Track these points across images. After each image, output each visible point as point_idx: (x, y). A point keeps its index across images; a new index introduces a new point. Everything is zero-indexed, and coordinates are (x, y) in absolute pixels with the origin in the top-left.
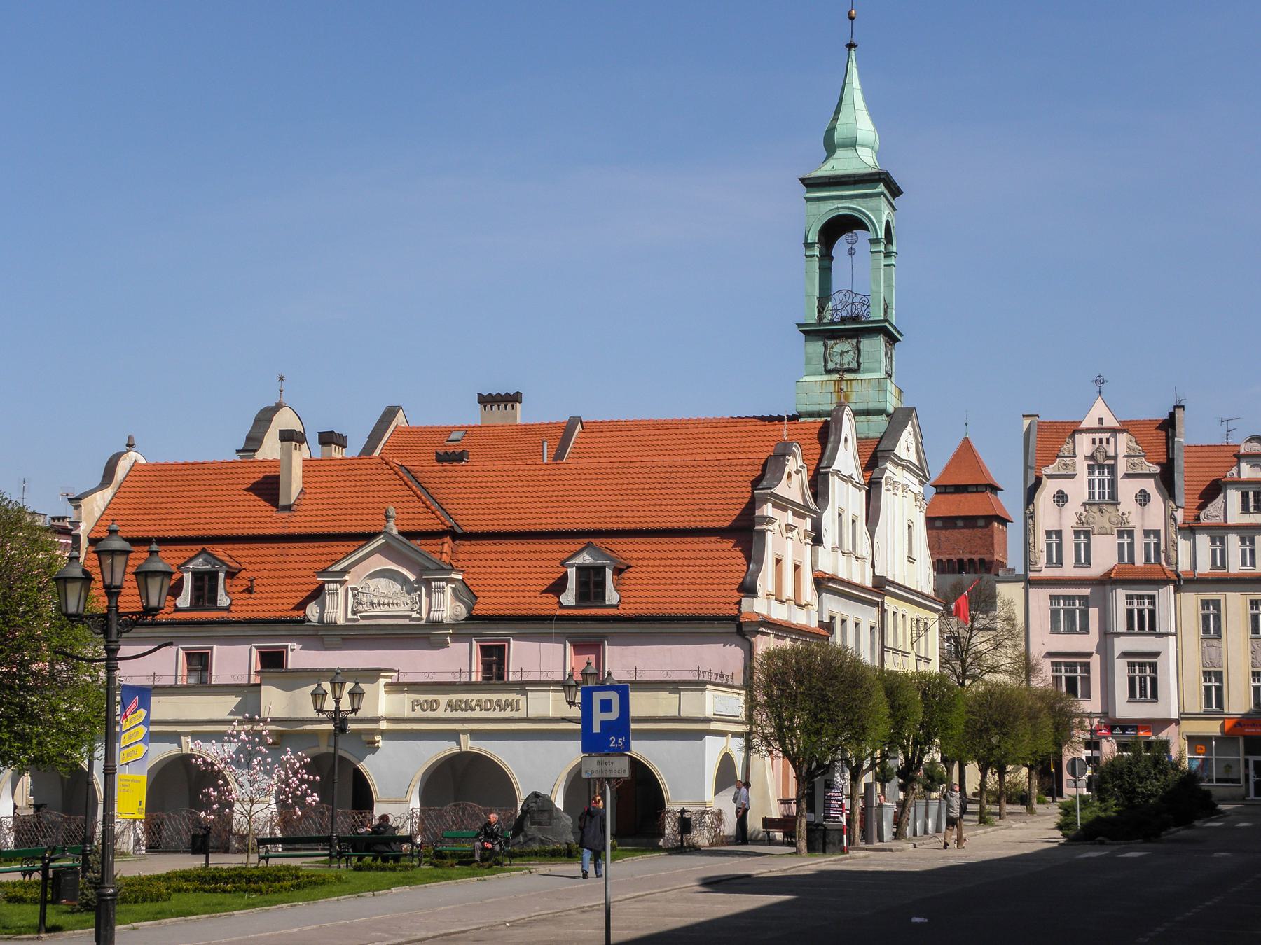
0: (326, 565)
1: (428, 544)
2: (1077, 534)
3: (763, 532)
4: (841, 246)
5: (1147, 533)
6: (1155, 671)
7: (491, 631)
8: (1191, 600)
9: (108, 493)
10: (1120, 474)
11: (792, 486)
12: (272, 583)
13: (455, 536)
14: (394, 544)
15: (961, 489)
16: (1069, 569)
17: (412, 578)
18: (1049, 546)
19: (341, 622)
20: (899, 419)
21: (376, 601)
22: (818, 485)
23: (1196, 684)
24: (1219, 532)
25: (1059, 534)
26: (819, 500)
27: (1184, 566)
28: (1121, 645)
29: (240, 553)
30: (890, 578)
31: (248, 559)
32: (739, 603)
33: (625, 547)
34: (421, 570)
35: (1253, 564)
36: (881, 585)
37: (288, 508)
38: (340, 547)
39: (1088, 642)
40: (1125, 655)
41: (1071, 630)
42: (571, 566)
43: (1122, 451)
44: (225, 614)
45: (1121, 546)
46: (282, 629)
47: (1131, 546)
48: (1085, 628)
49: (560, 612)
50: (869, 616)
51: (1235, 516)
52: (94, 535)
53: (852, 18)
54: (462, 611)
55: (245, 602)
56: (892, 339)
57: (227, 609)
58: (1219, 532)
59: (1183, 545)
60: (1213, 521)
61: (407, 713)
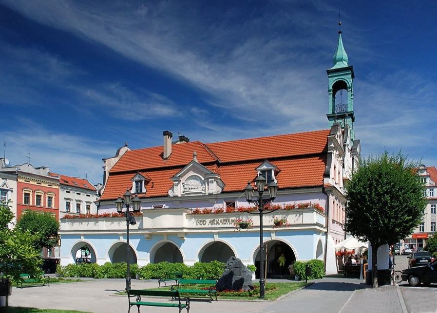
3: (331, 153)
9: (117, 159)
13: (220, 164)
17: (203, 179)
19: (179, 195)
21: (190, 187)
32: (323, 180)
33: (279, 164)
34: (205, 175)
35: (433, 195)
37: (166, 159)
44: (144, 195)
46: (161, 199)
52: (111, 172)
53: (340, 24)
54: (220, 190)
57: (145, 193)
61: (194, 226)
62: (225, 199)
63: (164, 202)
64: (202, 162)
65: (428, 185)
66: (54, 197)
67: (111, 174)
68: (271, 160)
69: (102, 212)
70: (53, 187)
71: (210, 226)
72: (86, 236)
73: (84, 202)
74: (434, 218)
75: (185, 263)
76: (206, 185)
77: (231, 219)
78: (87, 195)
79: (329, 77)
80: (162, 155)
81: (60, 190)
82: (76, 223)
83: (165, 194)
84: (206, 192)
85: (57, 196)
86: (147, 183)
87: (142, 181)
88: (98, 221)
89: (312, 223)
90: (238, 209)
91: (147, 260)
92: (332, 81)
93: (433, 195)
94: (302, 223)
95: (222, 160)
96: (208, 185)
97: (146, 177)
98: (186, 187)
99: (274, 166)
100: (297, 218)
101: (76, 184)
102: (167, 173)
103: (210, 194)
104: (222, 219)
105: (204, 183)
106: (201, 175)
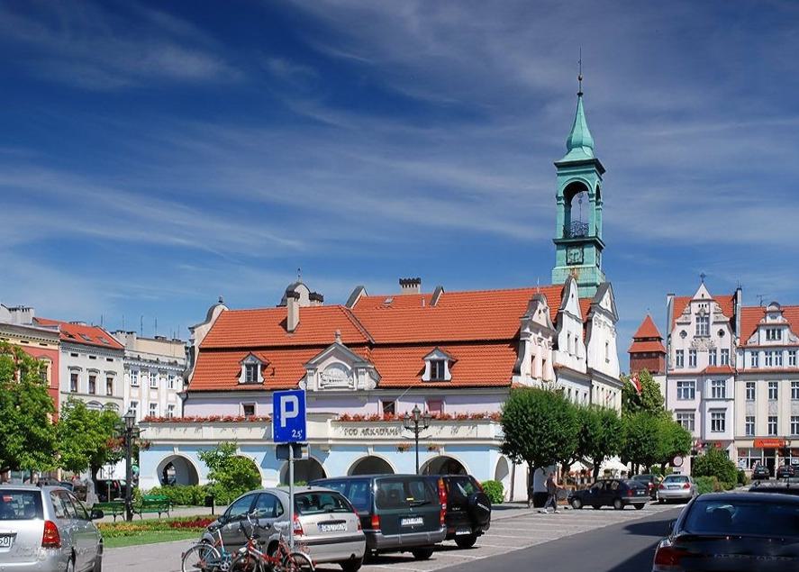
0: (307, 361)
1: (363, 348)
2: (690, 352)
3: (524, 341)
4: (575, 199)
5: (722, 351)
6: (724, 417)
7: (387, 394)
8: (742, 385)
9: (209, 326)
10: (711, 322)
11: (542, 317)
13: (371, 346)
14: (340, 349)
15: (645, 339)
16: (686, 369)
18: (678, 358)
20: (601, 290)
21: (331, 378)
22: (557, 322)
23: (742, 423)
24: (755, 350)
25: (682, 352)
26: (558, 327)
27: (739, 366)
28: (710, 405)
30: (596, 369)
35: (781, 364)
36: (591, 372)
37: (292, 332)
38: (316, 351)
39: (694, 404)
40: (711, 409)
41: (686, 397)
42: (427, 360)
43: (712, 311)
45: (710, 357)
47: (715, 357)
48: (693, 396)
50: (584, 389)
51: (764, 342)
52: (202, 346)
56: (599, 248)
57: (262, 383)
58: (755, 350)
59: (739, 358)
60: (753, 344)
61: (342, 436)
62: (381, 397)
64: (348, 342)
65: (786, 344)
66: (50, 366)
67: (202, 350)
69: (195, 410)
70: (49, 346)
71: (363, 437)
72: (181, 448)
73: (84, 369)
74: (794, 404)
76: (355, 376)
77: (389, 429)
78: (108, 360)
79: (558, 175)
80: (284, 324)
81: (60, 351)
82: (164, 429)
84: (355, 386)
85: (55, 362)
86: (264, 367)
89: (488, 437)
90: (400, 417)
91: (276, 480)
92: (565, 181)
93: (781, 364)
96: (357, 377)
97: (262, 358)
98: (325, 378)
101: (87, 338)
103: (361, 390)
106: (344, 361)
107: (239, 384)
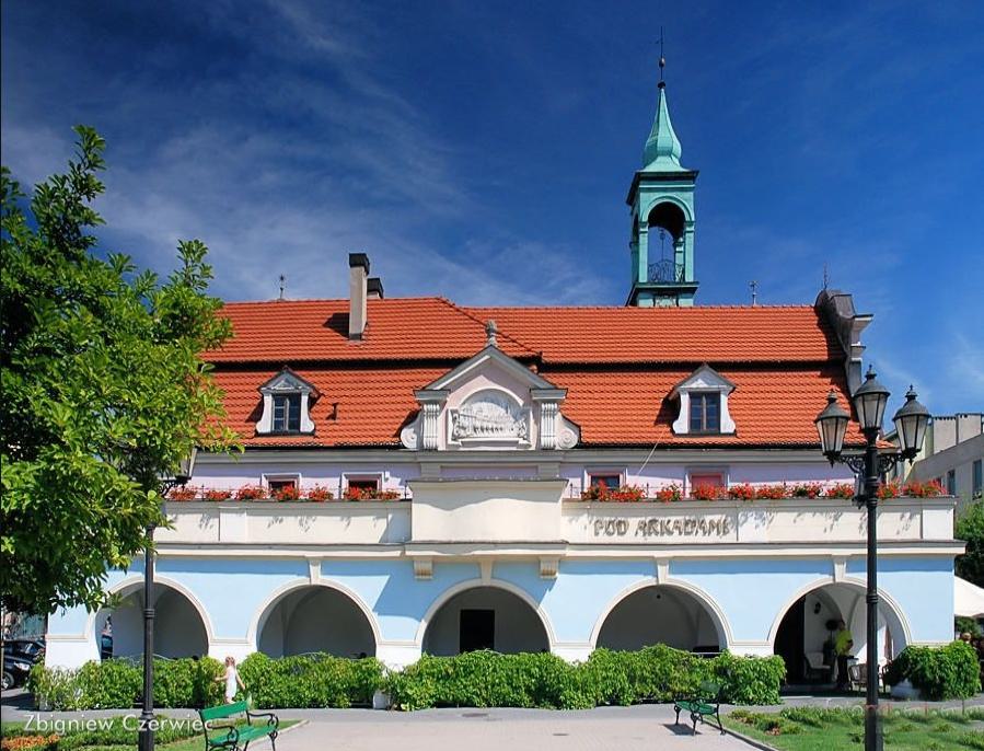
0: (424, 384)
12: (364, 407)
17: (521, 402)
21: (478, 424)
29: (316, 379)
31: (326, 386)
37: (358, 337)
44: (310, 439)
46: (376, 456)
49: (675, 440)
54: (574, 441)
55: (331, 428)
57: (312, 434)
61: (589, 537)
62: (588, 465)
63: (386, 465)
68: (719, 367)
71: (640, 539)
72: (329, 566)
75: (555, 651)
76: (532, 421)
77: (708, 519)
83: (390, 441)
87: (300, 395)
88: (219, 511)
94: (918, 537)
95: (546, 359)
96: (537, 422)
99: (309, 384)
100: (903, 523)
102: (373, 378)
104: (680, 518)
105: (524, 414)
106: (511, 390)
107: (258, 435)
